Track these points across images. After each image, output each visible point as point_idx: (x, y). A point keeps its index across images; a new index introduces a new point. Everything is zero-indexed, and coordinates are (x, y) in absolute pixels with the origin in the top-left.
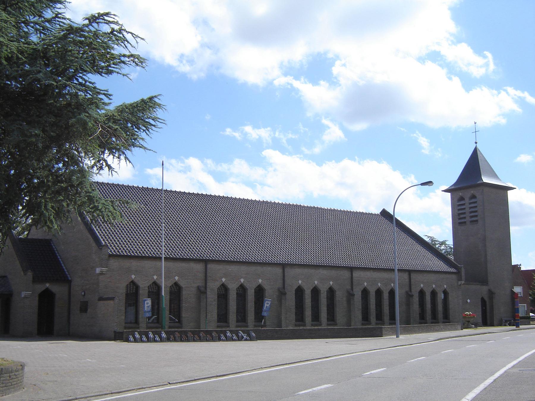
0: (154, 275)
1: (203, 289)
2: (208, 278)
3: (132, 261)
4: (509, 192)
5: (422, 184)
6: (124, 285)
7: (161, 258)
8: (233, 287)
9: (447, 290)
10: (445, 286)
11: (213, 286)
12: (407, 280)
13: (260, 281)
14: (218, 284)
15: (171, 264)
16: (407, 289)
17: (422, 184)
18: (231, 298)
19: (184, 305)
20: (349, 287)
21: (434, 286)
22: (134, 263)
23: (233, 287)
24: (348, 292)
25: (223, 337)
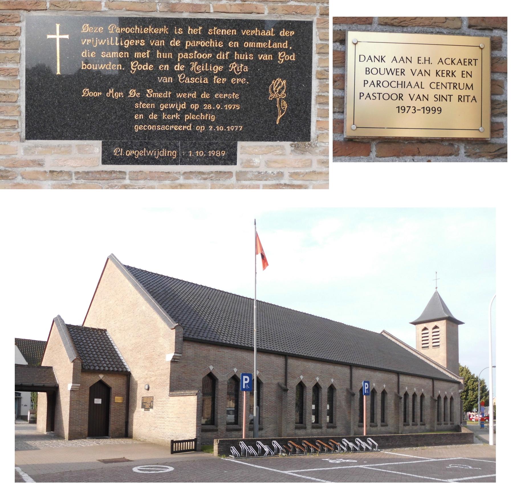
0: (234, 367)
1: (283, 386)
2: (288, 375)
3: (210, 348)
4: (460, 326)
5: (257, 236)
6: (201, 377)
7: (252, 350)
8: (309, 385)
9: (320, 383)
10: (384, 386)
11: (293, 383)
12: (431, 387)
13: (332, 380)
14: (297, 382)
15: (265, 357)
16: (431, 395)
17: (257, 236)
18: (307, 397)
19: (264, 403)
20: (396, 391)
21: (446, 393)
22: (213, 351)
23: (309, 385)
24: (396, 395)
25: (234, 450)
